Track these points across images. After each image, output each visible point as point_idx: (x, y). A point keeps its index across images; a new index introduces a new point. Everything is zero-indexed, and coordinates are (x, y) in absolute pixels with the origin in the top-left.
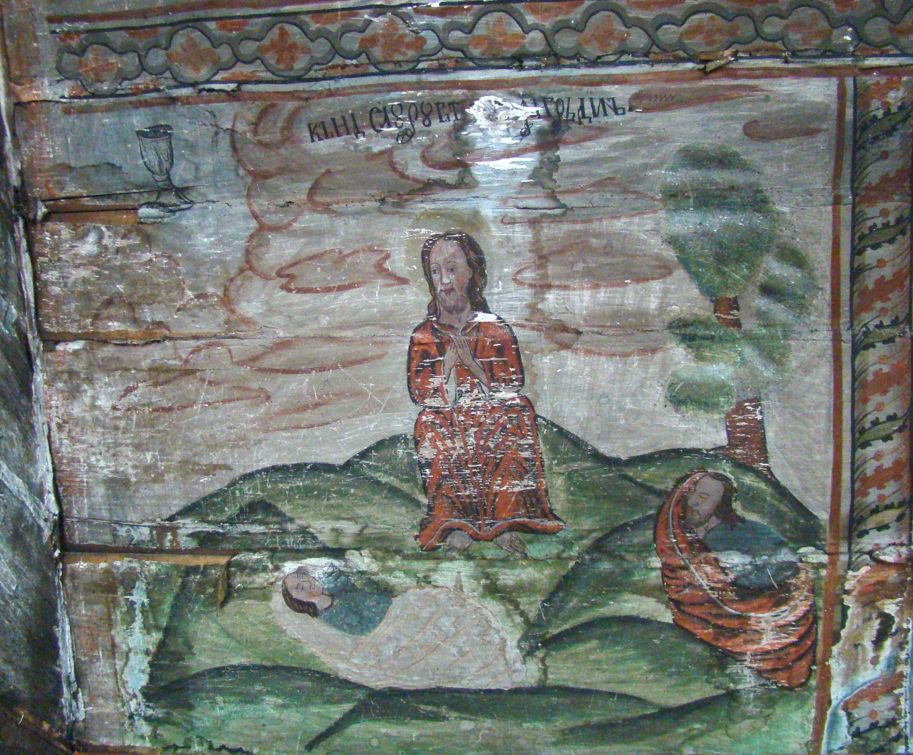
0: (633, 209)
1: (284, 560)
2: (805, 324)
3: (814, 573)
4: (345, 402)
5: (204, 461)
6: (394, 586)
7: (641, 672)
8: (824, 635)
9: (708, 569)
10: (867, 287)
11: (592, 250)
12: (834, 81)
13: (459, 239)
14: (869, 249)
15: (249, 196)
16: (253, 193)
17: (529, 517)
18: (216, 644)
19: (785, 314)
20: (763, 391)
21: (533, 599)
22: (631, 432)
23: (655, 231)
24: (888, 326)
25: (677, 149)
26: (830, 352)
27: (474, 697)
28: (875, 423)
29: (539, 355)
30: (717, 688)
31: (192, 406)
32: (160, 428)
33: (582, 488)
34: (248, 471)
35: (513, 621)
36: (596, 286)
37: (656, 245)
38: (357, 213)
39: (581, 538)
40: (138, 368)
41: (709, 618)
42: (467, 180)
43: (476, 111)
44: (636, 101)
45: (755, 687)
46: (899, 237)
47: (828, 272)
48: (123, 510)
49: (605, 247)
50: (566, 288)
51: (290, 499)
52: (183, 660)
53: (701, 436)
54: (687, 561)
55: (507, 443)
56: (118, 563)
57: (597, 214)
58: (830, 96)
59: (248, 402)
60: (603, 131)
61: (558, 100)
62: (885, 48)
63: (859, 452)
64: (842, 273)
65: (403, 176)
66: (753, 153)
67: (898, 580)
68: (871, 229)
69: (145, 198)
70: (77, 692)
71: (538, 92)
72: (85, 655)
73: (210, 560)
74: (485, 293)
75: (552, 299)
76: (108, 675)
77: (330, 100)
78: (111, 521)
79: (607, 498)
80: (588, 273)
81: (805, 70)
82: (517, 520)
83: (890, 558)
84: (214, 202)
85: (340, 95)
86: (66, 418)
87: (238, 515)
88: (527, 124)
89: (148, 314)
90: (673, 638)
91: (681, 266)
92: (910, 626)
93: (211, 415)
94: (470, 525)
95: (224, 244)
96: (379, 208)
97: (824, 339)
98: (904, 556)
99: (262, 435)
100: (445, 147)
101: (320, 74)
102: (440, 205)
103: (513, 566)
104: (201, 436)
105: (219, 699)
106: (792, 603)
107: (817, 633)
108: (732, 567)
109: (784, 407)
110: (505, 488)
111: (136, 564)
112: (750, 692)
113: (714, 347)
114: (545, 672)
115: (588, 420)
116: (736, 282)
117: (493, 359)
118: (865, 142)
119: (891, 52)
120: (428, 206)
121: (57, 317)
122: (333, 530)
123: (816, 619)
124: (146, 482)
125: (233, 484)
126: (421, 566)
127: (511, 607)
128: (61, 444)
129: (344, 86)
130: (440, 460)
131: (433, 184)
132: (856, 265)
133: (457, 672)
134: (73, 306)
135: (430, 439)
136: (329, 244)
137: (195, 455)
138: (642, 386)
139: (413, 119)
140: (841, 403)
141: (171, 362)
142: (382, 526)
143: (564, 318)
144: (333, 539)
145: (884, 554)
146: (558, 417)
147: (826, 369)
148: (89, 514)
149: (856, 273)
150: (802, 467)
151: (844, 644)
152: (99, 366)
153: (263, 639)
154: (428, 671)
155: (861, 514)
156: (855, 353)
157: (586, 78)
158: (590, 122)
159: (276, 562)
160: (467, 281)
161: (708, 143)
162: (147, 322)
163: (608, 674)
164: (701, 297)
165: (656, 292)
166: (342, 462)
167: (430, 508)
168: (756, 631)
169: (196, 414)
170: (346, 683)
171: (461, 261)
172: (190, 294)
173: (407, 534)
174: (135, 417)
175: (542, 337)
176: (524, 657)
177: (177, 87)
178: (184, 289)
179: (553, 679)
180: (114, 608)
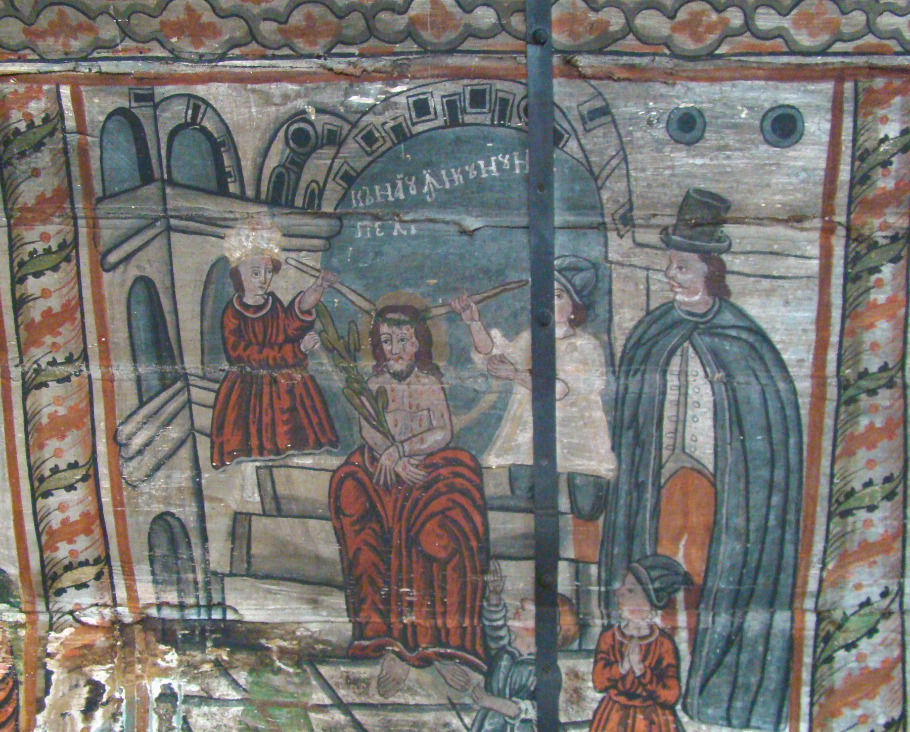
3: (11, 633)
8: (27, 702)
10: (33, 320)
14: (30, 277)
24: (62, 364)
28: (55, 470)
46: (63, 265)
62: (23, 52)
63: (41, 502)
67: (107, 644)
68: (31, 254)
83: (93, 620)
92: (123, 696)
98: (107, 618)
107: (18, 700)
118: (10, 158)
119: (29, 57)
123: (16, 683)
132: (18, 295)
140: (14, 449)
145: (85, 615)
151: (50, 713)
155: (54, 569)
156: (26, 391)
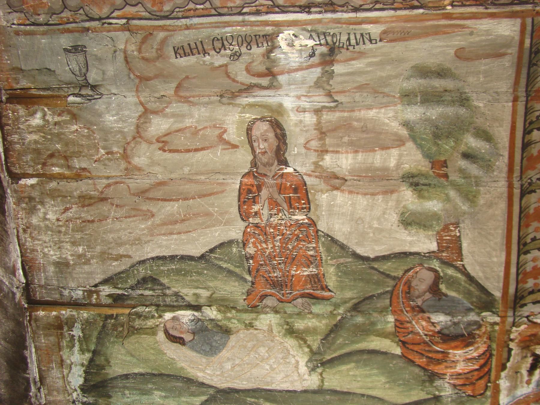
0: (381, 104)
1: (165, 311)
2: (491, 177)
4: (200, 220)
5: (115, 253)
6: (230, 328)
7: (381, 383)
8: (496, 366)
9: (424, 323)
10: (532, 155)
11: (355, 129)
12: (519, 21)
13: (270, 121)
14: (535, 130)
15: (137, 91)
16: (140, 89)
17: (314, 290)
18: (125, 361)
19: (477, 171)
20: (461, 218)
21: (315, 338)
22: (376, 241)
23: (396, 118)
25: (410, 66)
26: (506, 195)
27: (280, 394)
29: (320, 193)
30: (428, 394)
31: (106, 220)
32: (87, 232)
33: (345, 273)
34: (142, 259)
35: (303, 350)
36: (356, 152)
37: (395, 126)
38: (206, 104)
39: (346, 302)
40: (72, 195)
41: (424, 352)
42: (274, 84)
43: (282, 40)
44: (383, 37)
45: (451, 394)
47: (507, 145)
48: (66, 280)
49: (362, 128)
50: (337, 152)
51: (168, 276)
52: (104, 369)
53: (421, 245)
54: (411, 318)
55: (300, 246)
56: (64, 312)
57: (358, 107)
58: (515, 31)
59: (141, 218)
60: (362, 55)
61: (333, 34)
63: (522, 257)
64: (516, 145)
65: (234, 81)
66: (461, 68)
69: (72, 91)
70: (41, 388)
71: (320, 28)
72: (45, 367)
73: (120, 311)
74: (286, 155)
75: (328, 160)
76: (58, 378)
77: (187, 32)
78: (59, 287)
79: (362, 280)
80: (351, 143)
81: (499, 13)
82: (306, 291)
84: (115, 94)
85: (193, 29)
86: (28, 225)
87: (136, 285)
88: (313, 49)
89: (77, 163)
90: (401, 363)
91: (411, 139)
93: (118, 225)
94: (277, 294)
95: (123, 121)
96: (220, 100)
97: (502, 186)
99: (149, 238)
100: (260, 63)
101: (180, 15)
102: (258, 99)
103: (303, 318)
104: (112, 238)
105: (127, 392)
106: (476, 345)
107: (491, 365)
108: (439, 323)
109: (474, 228)
110: (298, 272)
111: (74, 313)
112: (448, 397)
113: (431, 190)
114: (322, 381)
115: (350, 233)
116: (446, 151)
117: (291, 195)
120: (251, 100)
121: (19, 164)
122: (195, 294)
123: (491, 355)
124: (80, 264)
125: (133, 266)
126: (247, 317)
127: (302, 342)
128: (26, 241)
129: (196, 22)
130: (258, 254)
131: (253, 87)
132: (526, 141)
133: (269, 379)
134: (29, 157)
135: (252, 243)
136: (188, 122)
137: (109, 248)
138: (384, 213)
139: (240, 45)
141: (92, 193)
142: (224, 293)
143: (336, 170)
144: (194, 299)
145: (536, 318)
146: (331, 231)
147: (503, 205)
148: (45, 282)
149: (526, 146)
150: (484, 265)
151: (509, 371)
152: (47, 194)
153: (153, 357)
154: (252, 378)
156: (522, 195)
157: (352, 19)
158: (354, 48)
159: (160, 313)
160: (275, 147)
161: (432, 62)
162: (77, 168)
163: (360, 383)
164: (423, 160)
165: (394, 156)
166: (199, 255)
167: (253, 283)
168: (453, 361)
169: (108, 224)
170: (202, 384)
171: (271, 135)
172: (102, 151)
173: (239, 297)
174: (71, 226)
175: (322, 182)
176: (310, 372)
177: (87, 21)
178: (98, 148)
179: (327, 385)
180: (62, 338)
